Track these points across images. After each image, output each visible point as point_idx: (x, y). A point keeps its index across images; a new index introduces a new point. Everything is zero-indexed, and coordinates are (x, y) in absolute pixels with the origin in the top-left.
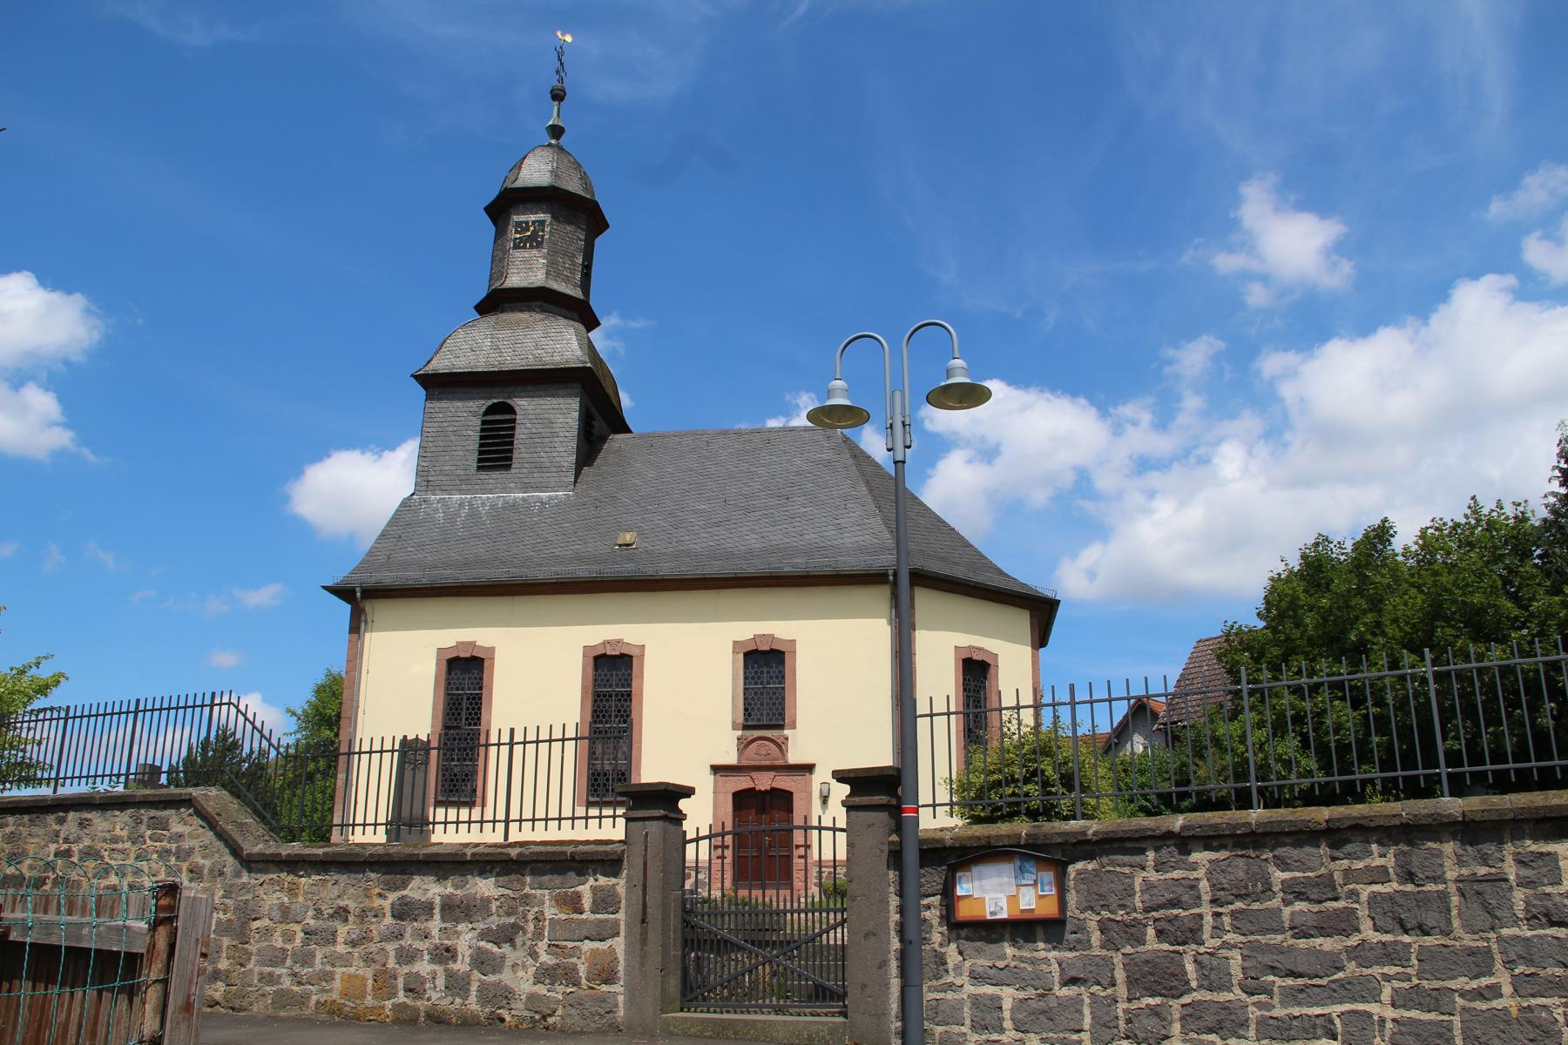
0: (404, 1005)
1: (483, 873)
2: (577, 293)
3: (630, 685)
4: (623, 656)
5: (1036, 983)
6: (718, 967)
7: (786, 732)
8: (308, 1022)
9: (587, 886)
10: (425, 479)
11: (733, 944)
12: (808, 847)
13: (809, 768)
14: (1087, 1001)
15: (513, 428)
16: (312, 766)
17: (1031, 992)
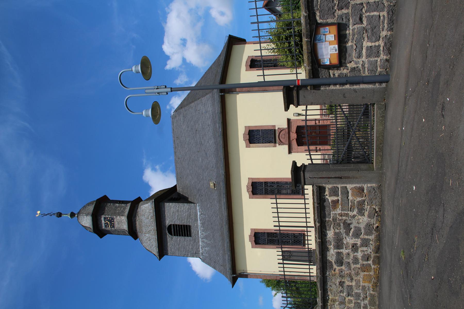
0: (373, 261)
1: (325, 235)
2: (129, 205)
3: (262, 182)
4: (252, 185)
5: (361, 33)
6: (357, 151)
7: (276, 128)
8: (380, 294)
9: (329, 198)
10: (196, 254)
11: (349, 146)
12: (315, 120)
13: (289, 120)
14: (368, 14)
15: (176, 225)
16: (294, 288)
17: (365, 35)
